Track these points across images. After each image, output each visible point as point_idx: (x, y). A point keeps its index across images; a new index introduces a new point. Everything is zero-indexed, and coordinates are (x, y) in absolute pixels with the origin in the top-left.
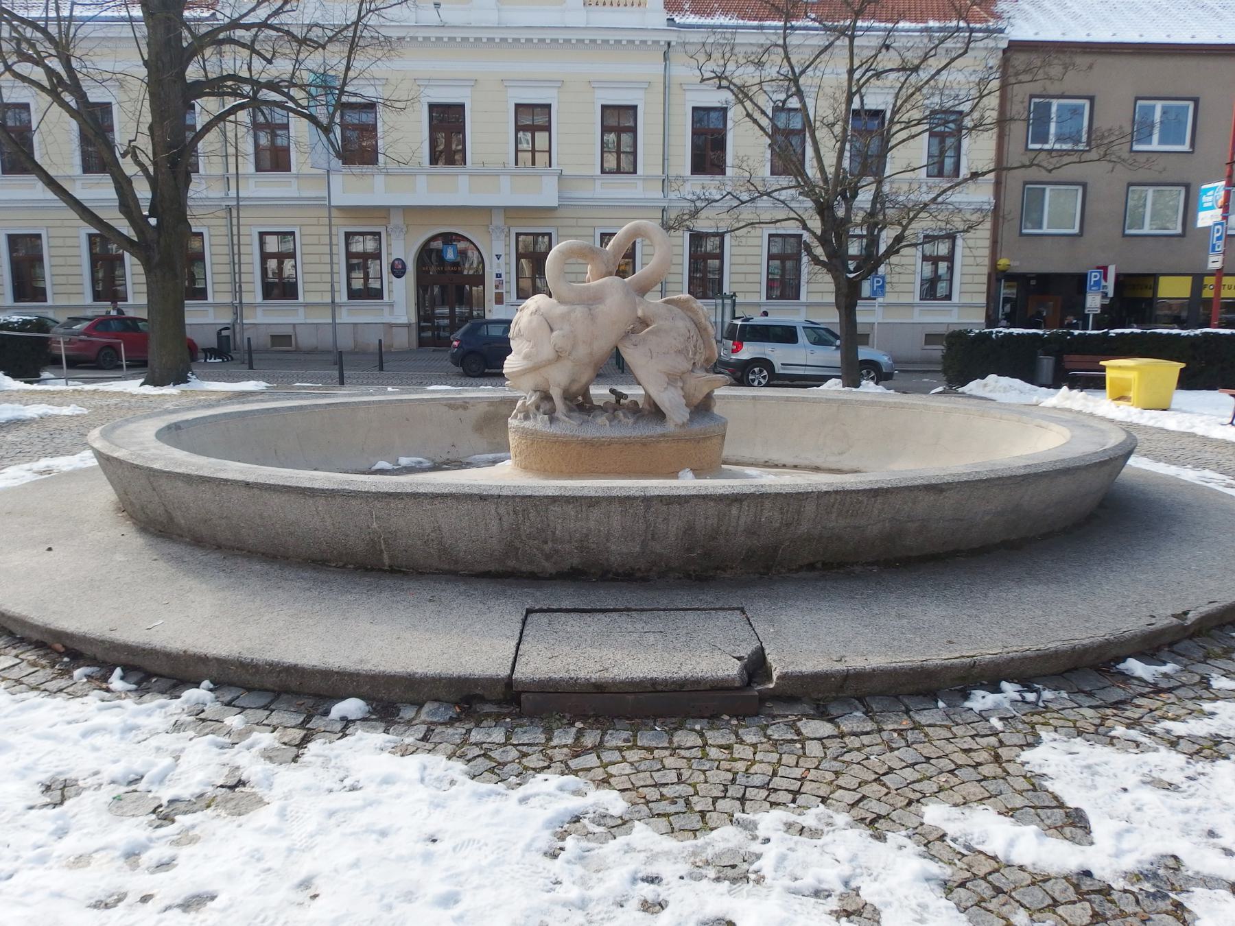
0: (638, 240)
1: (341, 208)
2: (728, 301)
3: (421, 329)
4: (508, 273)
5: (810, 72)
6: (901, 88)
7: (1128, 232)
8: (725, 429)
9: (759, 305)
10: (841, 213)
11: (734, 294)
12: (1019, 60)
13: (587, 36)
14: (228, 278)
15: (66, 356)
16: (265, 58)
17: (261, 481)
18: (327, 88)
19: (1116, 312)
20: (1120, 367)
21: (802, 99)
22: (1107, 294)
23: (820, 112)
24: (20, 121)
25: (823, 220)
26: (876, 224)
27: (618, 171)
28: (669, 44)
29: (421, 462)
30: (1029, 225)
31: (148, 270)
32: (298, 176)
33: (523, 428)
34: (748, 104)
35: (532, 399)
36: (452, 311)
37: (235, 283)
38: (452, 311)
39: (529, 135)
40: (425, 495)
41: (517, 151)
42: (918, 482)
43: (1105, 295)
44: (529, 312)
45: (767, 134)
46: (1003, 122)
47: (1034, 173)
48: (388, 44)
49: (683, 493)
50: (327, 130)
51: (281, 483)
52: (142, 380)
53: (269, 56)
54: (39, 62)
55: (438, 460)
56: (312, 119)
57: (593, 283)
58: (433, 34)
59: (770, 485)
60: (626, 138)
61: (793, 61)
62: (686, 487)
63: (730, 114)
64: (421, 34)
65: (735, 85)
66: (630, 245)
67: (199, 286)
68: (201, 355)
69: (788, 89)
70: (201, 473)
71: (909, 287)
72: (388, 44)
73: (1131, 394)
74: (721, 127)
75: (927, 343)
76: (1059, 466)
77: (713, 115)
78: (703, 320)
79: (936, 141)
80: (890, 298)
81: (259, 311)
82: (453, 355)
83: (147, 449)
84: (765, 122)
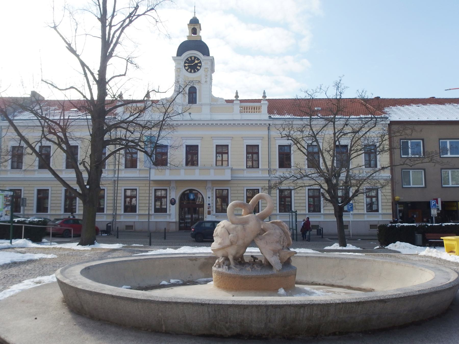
0: (260, 201)
1: (153, 181)
2: (294, 214)
3: (180, 223)
4: (212, 203)
5: (320, 134)
6: (353, 138)
7: (444, 186)
8: (296, 272)
9: (305, 215)
10: (334, 181)
11: (296, 211)
12: (394, 127)
13: (241, 123)
14: (112, 205)
15: (52, 233)
16: (131, 132)
17: (118, 295)
18: (151, 142)
19: (442, 217)
20: (449, 240)
21: (317, 142)
22: (439, 209)
23: (324, 147)
24: (47, 151)
25: (328, 185)
26: (348, 186)
27: (252, 167)
28: (270, 124)
29: (178, 282)
30: (405, 184)
31: (84, 203)
32: (140, 170)
33: (218, 271)
34: (298, 145)
35: (221, 260)
36: (192, 216)
37: (115, 207)
38: (192, 216)
39: (220, 155)
40: (180, 303)
41: (216, 161)
42: (376, 299)
43: (438, 209)
44: (221, 227)
45: (306, 155)
46: (391, 149)
47: (405, 166)
48: (172, 127)
49: (281, 304)
50: (150, 156)
51: (125, 296)
52: (78, 243)
53: (133, 131)
54: (55, 134)
55: (185, 281)
56: (146, 152)
57: (244, 216)
58: (188, 123)
59: (316, 301)
60: (255, 156)
61: (314, 130)
62: (282, 301)
63: (292, 148)
64: (184, 123)
65: (293, 139)
66: (257, 203)
67: (102, 207)
68: (100, 233)
69: (313, 139)
70: (95, 291)
71: (362, 208)
72: (172, 127)
73: (455, 250)
74: (289, 151)
75: (371, 228)
76: (432, 290)
77: (286, 148)
78: (286, 230)
79: (367, 155)
80: (355, 212)
81: (122, 217)
82: (192, 234)
83: (76, 279)
84: (305, 151)
